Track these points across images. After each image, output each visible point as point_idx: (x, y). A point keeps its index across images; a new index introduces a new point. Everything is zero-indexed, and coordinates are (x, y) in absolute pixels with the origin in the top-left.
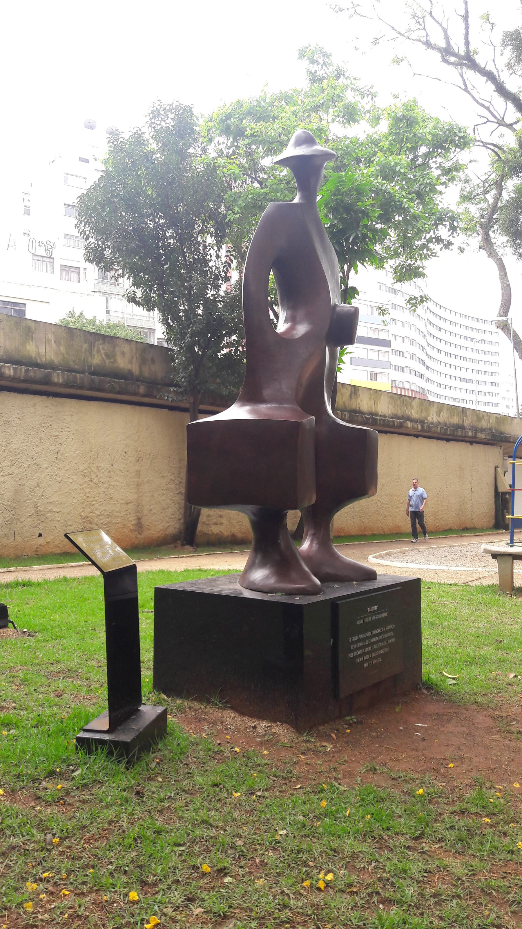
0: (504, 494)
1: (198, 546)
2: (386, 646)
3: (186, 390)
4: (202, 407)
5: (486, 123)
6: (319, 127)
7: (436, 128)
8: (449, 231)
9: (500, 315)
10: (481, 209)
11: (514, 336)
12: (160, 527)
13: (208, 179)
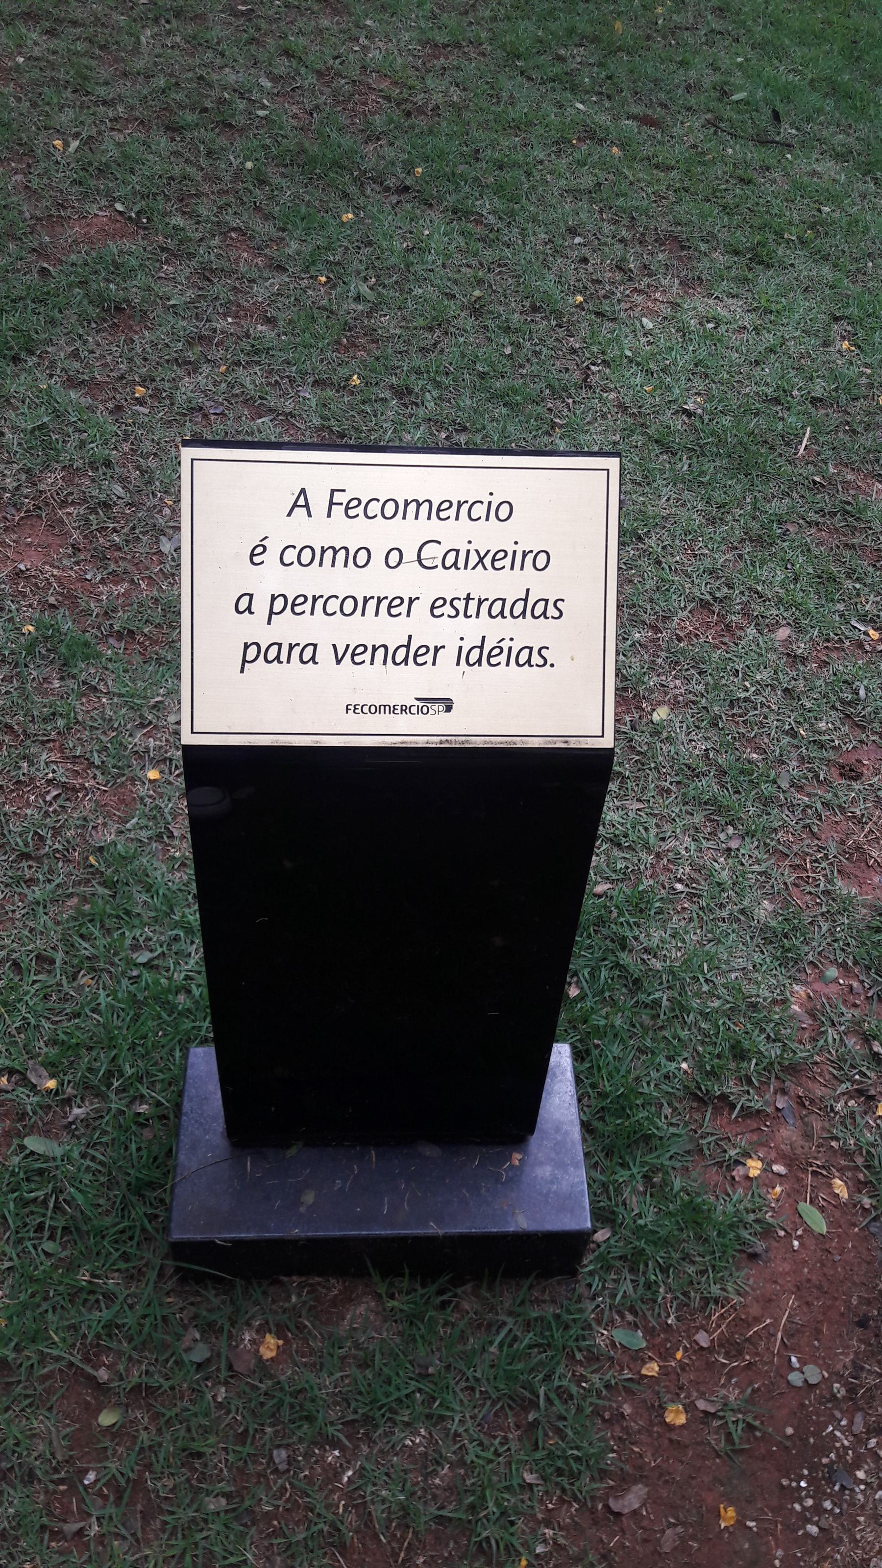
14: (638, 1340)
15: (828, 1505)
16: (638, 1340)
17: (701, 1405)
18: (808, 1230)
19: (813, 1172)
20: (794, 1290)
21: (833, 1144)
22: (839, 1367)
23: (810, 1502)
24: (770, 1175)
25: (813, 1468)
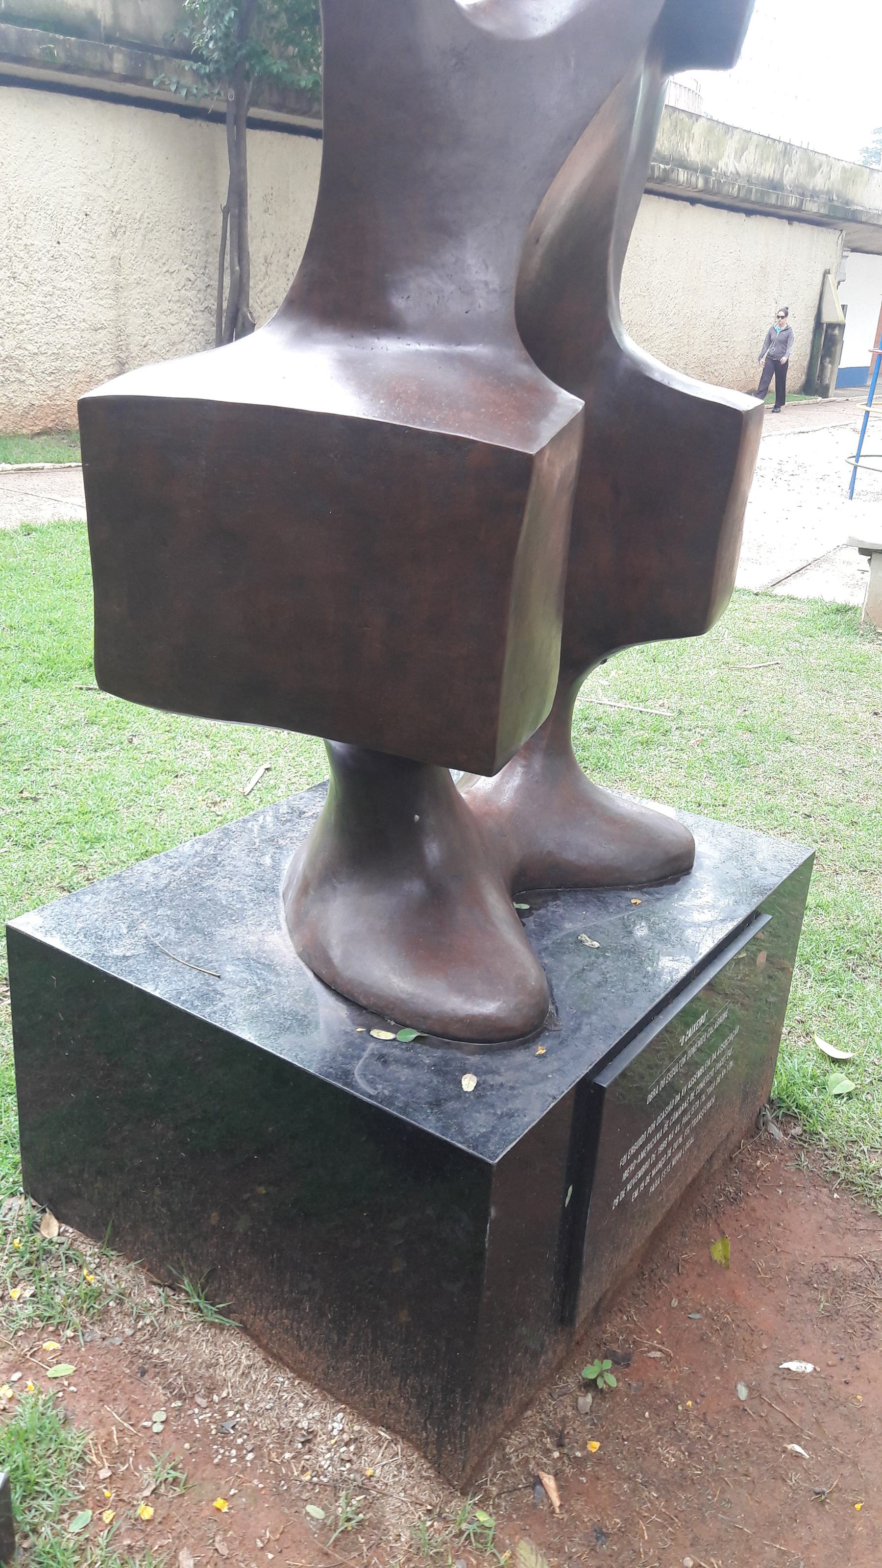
0: (832, 326)
3: (218, 71)
4: (255, 112)
14: (85, 1516)
15: (240, 1441)
16: (85, 1516)
17: (147, 1493)
18: (67, 1378)
19: (31, 1356)
20: (101, 1403)
21: (19, 1334)
22: (163, 1398)
23: (234, 1452)
24: (16, 1385)
25: (214, 1442)
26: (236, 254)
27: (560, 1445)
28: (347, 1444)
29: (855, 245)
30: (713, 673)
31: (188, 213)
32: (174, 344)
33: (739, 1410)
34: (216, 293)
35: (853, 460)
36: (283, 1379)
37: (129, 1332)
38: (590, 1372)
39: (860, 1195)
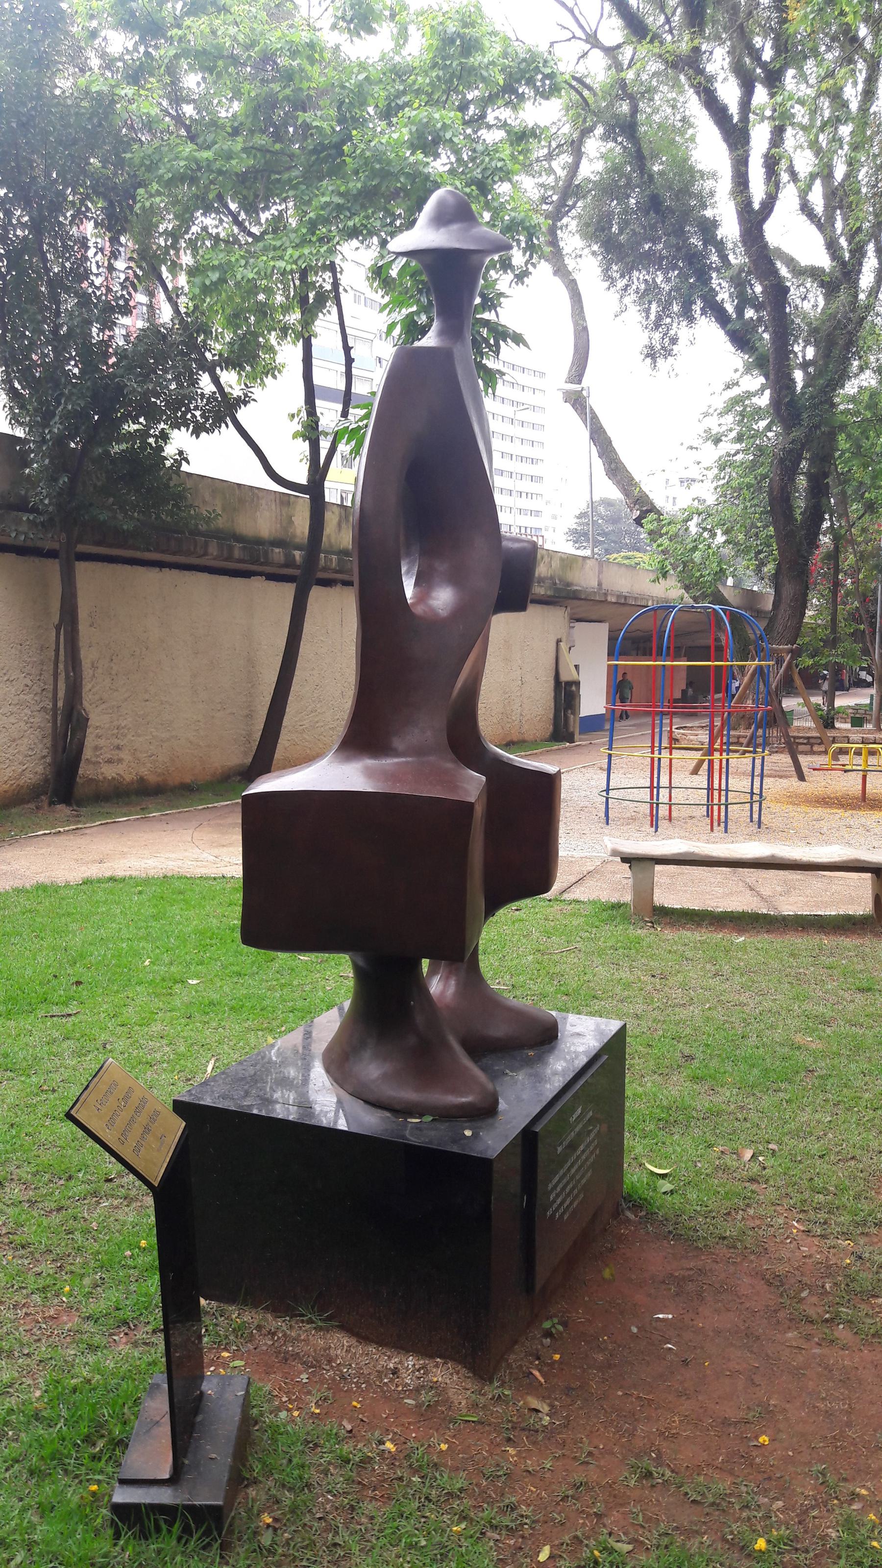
0: (569, 684)
1: (80, 803)
2: (587, 1171)
3: (51, 520)
4: (81, 548)
5: (569, 40)
6: (311, 41)
7: (505, 55)
8: (524, 255)
9: (570, 380)
10: (542, 185)
11: (592, 419)
12: (9, 773)
13: (100, 125)
26: (70, 663)
27: (538, 1358)
28: (418, 1370)
29: (577, 616)
30: (530, 958)
31: (25, 631)
32: (14, 740)
33: (635, 1337)
34: (50, 695)
35: (604, 794)
36: (372, 1349)
37: (270, 1343)
38: (547, 1325)
39: (686, 1240)
